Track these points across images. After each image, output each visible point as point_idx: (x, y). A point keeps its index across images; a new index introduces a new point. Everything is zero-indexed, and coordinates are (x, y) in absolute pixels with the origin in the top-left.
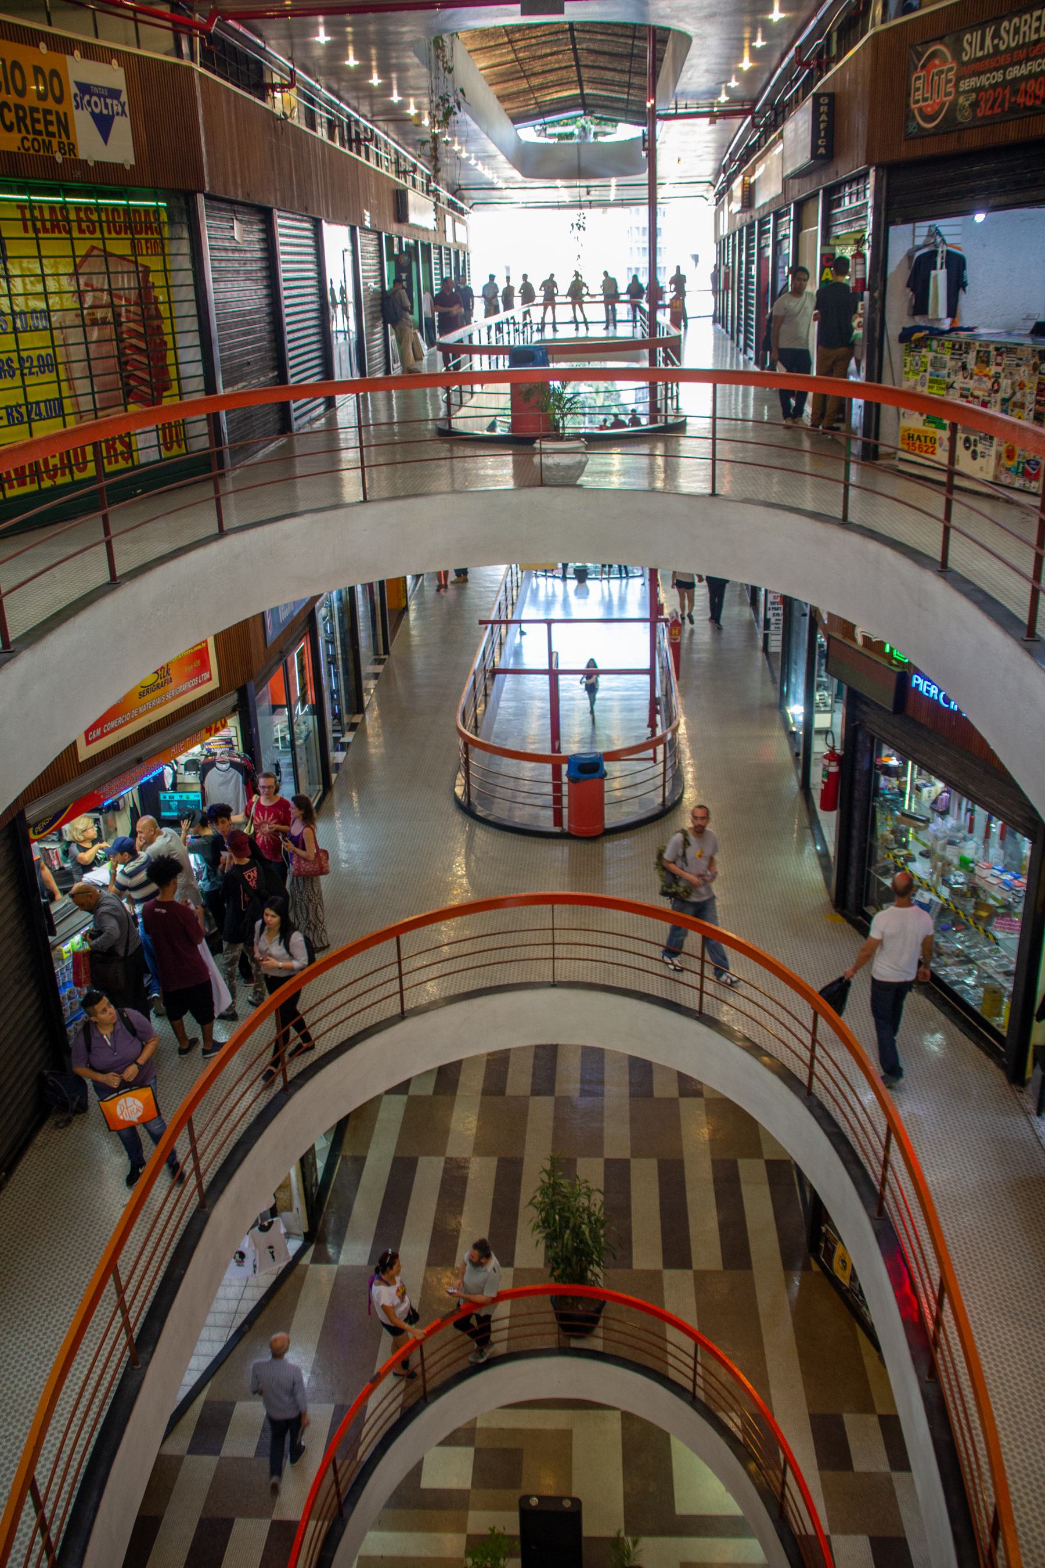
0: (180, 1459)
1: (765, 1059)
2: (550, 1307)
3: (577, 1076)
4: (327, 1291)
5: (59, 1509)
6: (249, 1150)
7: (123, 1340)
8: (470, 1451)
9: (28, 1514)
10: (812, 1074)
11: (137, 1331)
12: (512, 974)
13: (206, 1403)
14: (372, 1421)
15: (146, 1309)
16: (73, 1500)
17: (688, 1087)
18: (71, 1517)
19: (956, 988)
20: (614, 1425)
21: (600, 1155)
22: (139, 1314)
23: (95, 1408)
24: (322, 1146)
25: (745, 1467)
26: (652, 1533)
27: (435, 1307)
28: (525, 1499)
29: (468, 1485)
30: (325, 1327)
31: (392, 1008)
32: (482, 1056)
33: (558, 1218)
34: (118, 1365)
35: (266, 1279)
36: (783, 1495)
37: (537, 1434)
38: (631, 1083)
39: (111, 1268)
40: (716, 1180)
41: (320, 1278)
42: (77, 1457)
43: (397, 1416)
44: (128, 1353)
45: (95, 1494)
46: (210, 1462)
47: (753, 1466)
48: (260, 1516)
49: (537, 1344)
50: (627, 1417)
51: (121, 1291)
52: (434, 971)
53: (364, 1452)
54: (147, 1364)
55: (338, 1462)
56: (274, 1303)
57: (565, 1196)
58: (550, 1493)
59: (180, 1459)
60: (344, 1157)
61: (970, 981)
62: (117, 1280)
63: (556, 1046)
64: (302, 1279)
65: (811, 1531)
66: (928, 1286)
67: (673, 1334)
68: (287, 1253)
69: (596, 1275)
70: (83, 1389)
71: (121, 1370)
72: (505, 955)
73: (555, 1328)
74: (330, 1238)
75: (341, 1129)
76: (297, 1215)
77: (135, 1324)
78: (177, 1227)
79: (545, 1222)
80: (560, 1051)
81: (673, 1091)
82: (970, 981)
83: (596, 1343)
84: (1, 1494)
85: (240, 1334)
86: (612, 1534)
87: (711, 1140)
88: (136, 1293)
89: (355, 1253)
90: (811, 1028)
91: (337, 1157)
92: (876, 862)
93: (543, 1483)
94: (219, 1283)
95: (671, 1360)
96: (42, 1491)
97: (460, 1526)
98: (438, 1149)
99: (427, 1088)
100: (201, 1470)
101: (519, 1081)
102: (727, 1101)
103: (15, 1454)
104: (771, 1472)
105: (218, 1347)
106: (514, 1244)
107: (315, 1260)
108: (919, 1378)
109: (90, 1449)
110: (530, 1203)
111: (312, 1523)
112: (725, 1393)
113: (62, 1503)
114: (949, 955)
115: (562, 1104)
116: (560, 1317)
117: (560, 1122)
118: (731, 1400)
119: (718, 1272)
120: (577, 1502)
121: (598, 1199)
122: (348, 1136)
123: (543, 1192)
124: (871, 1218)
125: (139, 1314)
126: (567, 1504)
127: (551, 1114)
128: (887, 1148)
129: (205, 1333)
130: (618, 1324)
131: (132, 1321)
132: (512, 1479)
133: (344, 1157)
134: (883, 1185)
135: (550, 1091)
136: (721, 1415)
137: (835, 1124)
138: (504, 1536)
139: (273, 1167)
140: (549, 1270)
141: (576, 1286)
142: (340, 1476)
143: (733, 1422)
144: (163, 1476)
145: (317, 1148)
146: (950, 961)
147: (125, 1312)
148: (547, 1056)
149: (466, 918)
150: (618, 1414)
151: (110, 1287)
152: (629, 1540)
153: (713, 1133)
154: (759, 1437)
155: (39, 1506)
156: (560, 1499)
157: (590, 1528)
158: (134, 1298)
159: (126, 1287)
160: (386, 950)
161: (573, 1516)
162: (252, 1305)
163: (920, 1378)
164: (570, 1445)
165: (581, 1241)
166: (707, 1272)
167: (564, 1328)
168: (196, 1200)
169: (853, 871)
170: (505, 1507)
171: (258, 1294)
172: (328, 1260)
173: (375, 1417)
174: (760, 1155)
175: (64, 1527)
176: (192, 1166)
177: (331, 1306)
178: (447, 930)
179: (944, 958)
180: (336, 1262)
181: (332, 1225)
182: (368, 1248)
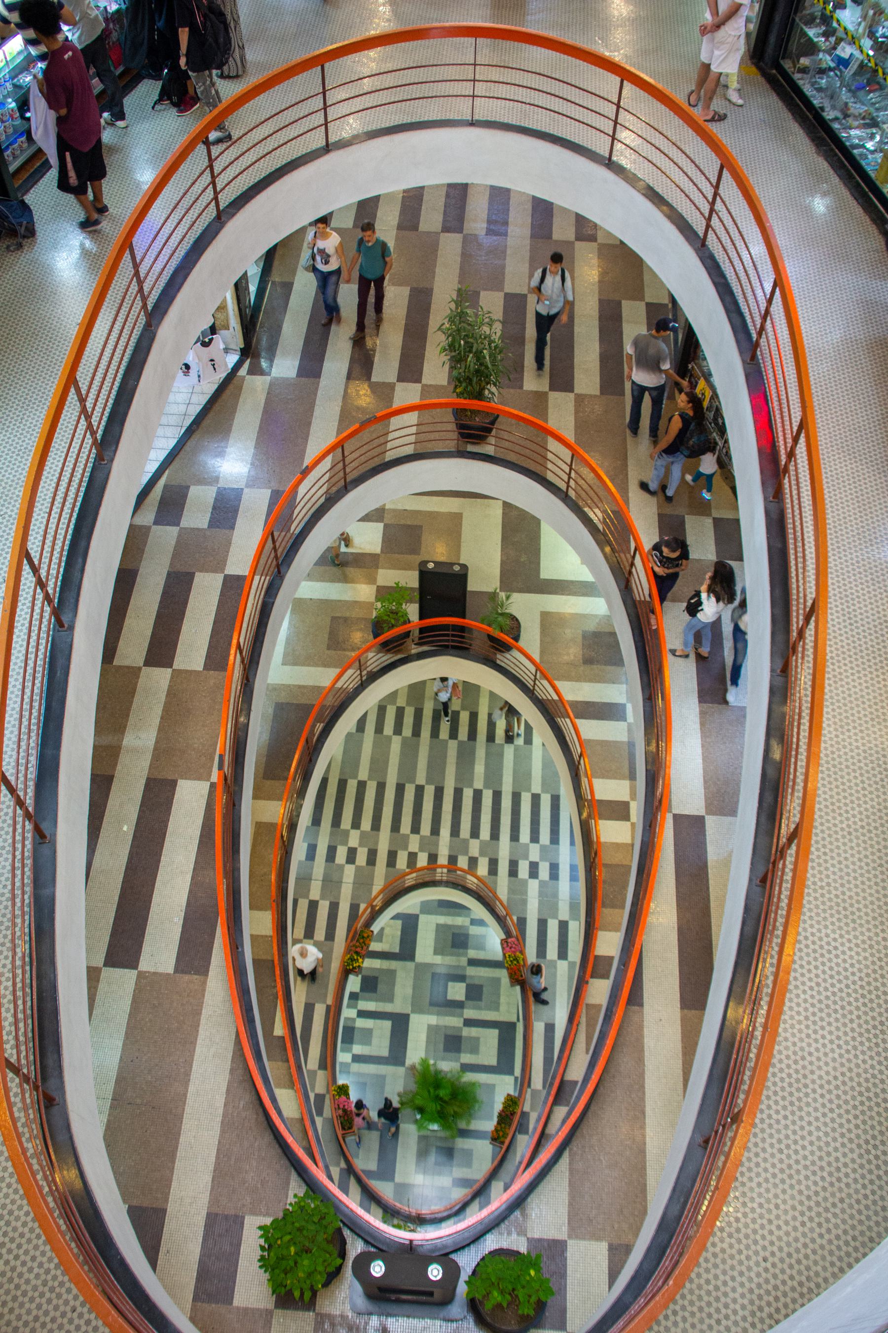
0: (148, 529)
1: (665, 208)
2: (452, 419)
3: (484, 216)
4: (262, 398)
5: (53, 571)
6: (188, 274)
7: (89, 440)
8: (381, 526)
9: (27, 579)
10: (708, 226)
12: (432, 111)
13: (165, 486)
14: (302, 504)
15: (106, 414)
16: (63, 564)
17: (585, 229)
18: (63, 576)
19: (855, 152)
20: (497, 511)
21: (502, 290)
22: (101, 419)
23: (72, 495)
24: (254, 272)
25: (603, 551)
26: (521, 591)
27: (354, 414)
28: (424, 563)
29: (378, 550)
30: (260, 428)
31: (316, 140)
33: (463, 347)
34: (86, 465)
35: (209, 387)
36: (630, 573)
37: (433, 516)
38: (533, 226)
39: (71, 380)
40: (601, 318)
41: (255, 389)
42: (62, 532)
43: (322, 500)
44: (94, 451)
45: (80, 560)
46: (172, 532)
47: (608, 549)
48: (215, 571)
49: (440, 447)
50: (507, 505)
51: (82, 400)
52: (358, 104)
53: (296, 527)
54: (112, 460)
55: (276, 534)
56: (217, 407)
57: (469, 325)
58: (442, 559)
59: (148, 529)
60: (274, 283)
61: (870, 145)
63: (466, 185)
64: (240, 388)
66: (787, 423)
67: (553, 445)
68: (226, 365)
69: (493, 394)
70: (59, 479)
71: (90, 465)
72: (426, 90)
73: (455, 435)
74: (263, 354)
75: (270, 256)
76: (233, 335)
77: (98, 427)
78: (127, 344)
79: (452, 347)
80: (470, 191)
81: (570, 235)
82: (870, 145)
83: (489, 449)
84: (1, 569)
85: (190, 431)
86: (491, 590)
87: (600, 282)
88: (96, 400)
89: (285, 366)
90: (714, 182)
91: (266, 283)
92: (804, 8)
93: (437, 552)
94: (169, 391)
95: (550, 465)
96: (84, 392)
97: (372, 580)
100: (165, 538)
103: (9, 534)
104: (622, 555)
105: (172, 443)
106: (422, 363)
107: (252, 371)
108: (765, 499)
109: (72, 526)
110: (439, 329)
111: (257, 578)
112: (591, 493)
113: (54, 566)
114: (856, 117)
115: (469, 241)
116: (461, 426)
117: (466, 256)
118: (596, 499)
119: (595, 396)
120: (464, 567)
121: (498, 328)
122: (276, 263)
123: (451, 320)
124: (744, 362)
125: (101, 419)
126: (457, 568)
127: (459, 251)
128: (770, 301)
129: (160, 431)
130: (507, 436)
131: (95, 424)
132: (414, 549)
133: (274, 283)
134: (760, 334)
135: (460, 230)
136: (586, 509)
137: (722, 275)
138: (406, 589)
139: (209, 292)
140: (453, 386)
141: (475, 402)
142: (277, 544)
143: (596, 515)
144: (136, 542)
145: (249, 274)
146: (856, 123)
147: (88, 418)
148: (458, 194)
149: (388, 48)
150: (500, 503)
151: (72, 395)
152: (503, 595)
153: (603, 275)
154: (616, 528)
155: (35, 570)
156: (453, 564)
157: (473, 585)
158: (95, 405)
159: (87, 396)
160: (309, 80)
161: (462, 577)
162: (198, 408)
163: (765, 499)
164: (461, 524)
165: (481, 364)
166: (586, 395)
167: (463, 436)
168: (142, 320)
169: (777, 18)
170: (406, 567)
171: (204, 399)
172: (262, 373)
173: (305, 500)
174: (642, 298)
175: (59, 583)
176: (136, 288)
177: (266, 411)
178: (370, 60)
179: (850, 120)
180: (269, 374)
181: (264, 342)
182: (297, 363)
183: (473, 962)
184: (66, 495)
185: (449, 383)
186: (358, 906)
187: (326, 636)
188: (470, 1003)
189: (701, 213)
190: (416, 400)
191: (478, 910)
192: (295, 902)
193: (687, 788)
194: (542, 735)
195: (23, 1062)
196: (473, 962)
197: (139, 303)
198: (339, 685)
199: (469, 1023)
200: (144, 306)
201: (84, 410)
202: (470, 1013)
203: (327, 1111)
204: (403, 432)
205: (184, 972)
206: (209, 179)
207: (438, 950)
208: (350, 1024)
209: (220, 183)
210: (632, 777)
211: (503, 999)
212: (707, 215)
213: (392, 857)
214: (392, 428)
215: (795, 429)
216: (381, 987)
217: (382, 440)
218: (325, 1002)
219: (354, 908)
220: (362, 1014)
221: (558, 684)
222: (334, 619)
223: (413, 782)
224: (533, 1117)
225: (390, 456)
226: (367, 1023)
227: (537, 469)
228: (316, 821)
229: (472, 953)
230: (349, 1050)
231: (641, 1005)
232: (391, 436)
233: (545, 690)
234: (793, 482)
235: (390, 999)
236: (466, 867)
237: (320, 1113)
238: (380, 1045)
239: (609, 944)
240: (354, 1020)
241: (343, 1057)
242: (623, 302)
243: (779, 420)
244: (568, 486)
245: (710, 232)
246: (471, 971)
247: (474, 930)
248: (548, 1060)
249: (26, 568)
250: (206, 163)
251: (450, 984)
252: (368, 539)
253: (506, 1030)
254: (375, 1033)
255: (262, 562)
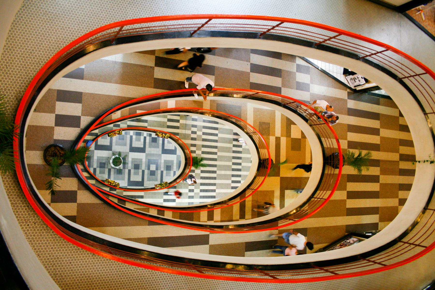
1: (411, 228)
5: (277, 31)
7: (321, 40)
8: (300, 138)
10: (405, 243)
11: (268, 33)
17: (402, 202)
24: (382, 92)
29: (292, 137)
32: (411, 138)
36: (287, 219)
39: (341, 33)
46: (294, 70)
51: (334, 37)
55: (295, 103)
62: (337, 36)
65: (279, 225)
67: (329, 192)
90: (420, 244)
91: (379, 96)
95: (322, 192)
96: (280, 26)
98: (382, 127)
99: (401, 122)
101: (404, 150)
102: (397, 214)
118: (311, 207)
122: (386, 100)
128: (379, 263)
136: (307, 205)
143: (306, 207)
147: (329, 40)
155: (277, 26)
183: (162, 172)
184: (303, 34)
185: (55, 140)
186: (178, 135)
187: (264, 121)
188: (149, 172)
189: (409, 240)
190: (342, 147)
191: (178, 173)
192: (179, 115)
193: (216, 238)
194: (234, 192)
195: (124, 32)
196: (162, 172)
197: (368, 54)
198: (248, 126)
199: (143, 172)
200: (367, 56)
201: (331, 38)
202: (146, 172)
203: (115, 128)
204: (327, 143)
205: (155, 81)
206: (412, 75)
207: (99, 158)
208: (142, 134)
209: (411, 78)
210: (222, 221)
211: (151, 182)
212: (409, 242)
213: (194, 145)
214: (332, 140)
215: (336, 272)
216: (153, 143)
217: (328, 137)
218: (148, 126)
219: (178, 134)
220: (145, 138)
221: (251, 196)
222: (269, 124)
223: (197, 150)
224: (115, 192)
225: (323, 139)
226: (142, 140)
227: (321, 188)
228: (204, 121)
229: (165, 172)
230: (134, 134)
231: (149, 225)
232: (329, 140)
233: (248, 193)
234: (318, 272)
235: (150, 147)
236: (99, 143)
237: (114, 126)
238: (136, 144)
239: (168, 215)
240: (143, 135)
241: (132, 133)
242: (378, 215)
243: (334, 267)
244: (315, 198)
245: (403, 243)
246: (159, 172)
247: (172, 172)
248: (132, 196)
249: (279, 22)
250: (418, 73)
251: (155, 165)
252: (295, 134)
253: (141, 183)
254: (139, 142)
255: (286, 99)
